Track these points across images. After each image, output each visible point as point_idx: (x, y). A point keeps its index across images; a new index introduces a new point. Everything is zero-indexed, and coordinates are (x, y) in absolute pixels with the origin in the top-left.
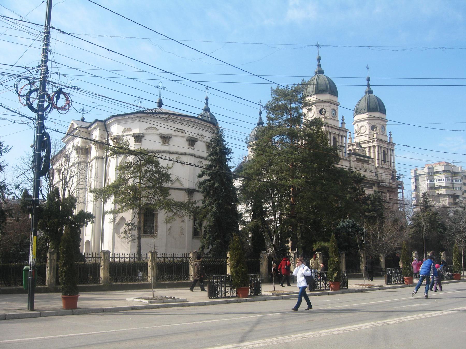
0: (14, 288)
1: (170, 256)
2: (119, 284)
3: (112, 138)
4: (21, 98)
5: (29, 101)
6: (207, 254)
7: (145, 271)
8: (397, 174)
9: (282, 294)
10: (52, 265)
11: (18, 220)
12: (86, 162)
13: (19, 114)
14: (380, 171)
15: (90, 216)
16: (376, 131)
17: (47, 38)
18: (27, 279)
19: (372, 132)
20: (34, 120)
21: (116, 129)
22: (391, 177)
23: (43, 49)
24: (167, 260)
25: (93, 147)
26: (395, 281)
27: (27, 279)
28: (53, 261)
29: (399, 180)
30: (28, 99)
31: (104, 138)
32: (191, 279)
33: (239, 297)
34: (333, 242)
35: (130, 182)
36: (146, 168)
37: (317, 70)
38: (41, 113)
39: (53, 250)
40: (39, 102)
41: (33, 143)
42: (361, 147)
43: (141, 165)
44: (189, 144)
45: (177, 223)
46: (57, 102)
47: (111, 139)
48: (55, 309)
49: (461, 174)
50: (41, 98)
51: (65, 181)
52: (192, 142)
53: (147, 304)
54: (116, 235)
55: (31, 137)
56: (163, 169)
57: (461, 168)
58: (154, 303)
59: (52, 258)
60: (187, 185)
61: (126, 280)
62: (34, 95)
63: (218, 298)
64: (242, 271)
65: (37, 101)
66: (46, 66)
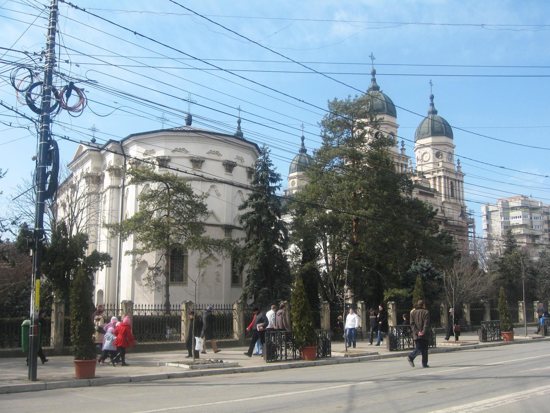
0: (10, 350)
1: (220, 308)
2: (146, 343)
3: (131, 162)
4: (20, 94)
5: (31, 98)
6: (251, 305)
7: (177, 328)
8: (467, 210)
9: (358, 355)
10: (59, 320)
11: (13, 265)
12: (98, 194)
13: (16, 112)
14: (446, 206)
15: (106, 258)
16: (441, 158)
17: (55, 15)
18: (27, 338)
19: (438, 160)
20: (37, 123)
21: (135, 151)
22: (460, 213)
23: (49, 29)
24: (222, 312)
25: (107, 174)
26: (491, 337)
27: (27, 338)
28: (60, 314)
29: (469, 217)
30: (29, 95)
31: (120, 164)
32: (236, 337)
33: (304, 359)
34: (419, 287)
35: (155, 216)
36: (175, 198)
37: (371, 86)
38: (45, 114)
39: (59, 300)
40: (44, 99)
41: (35, 155)
42: (424, 177)
43: (170, 194)
44: (227, 169)
45: (211, 269)
46: (67, 101)
47: (130, 163)
48: (65, 379)
49: (541, 211)
50: (46, 94)
51: (73, 216)
52: (230, 166)
53: (187, 369)
54: (136, 282)
55: (32, 145)
56: (196, 199)
57: (541, 203)
58: (197, 368)
59: (59, 311)
60: (224, 220)
61: (154, 339)
62: (37, 90)
63: (277, 361)
64: (308, 326)
65: (40, 99)
66: (52, 51)
